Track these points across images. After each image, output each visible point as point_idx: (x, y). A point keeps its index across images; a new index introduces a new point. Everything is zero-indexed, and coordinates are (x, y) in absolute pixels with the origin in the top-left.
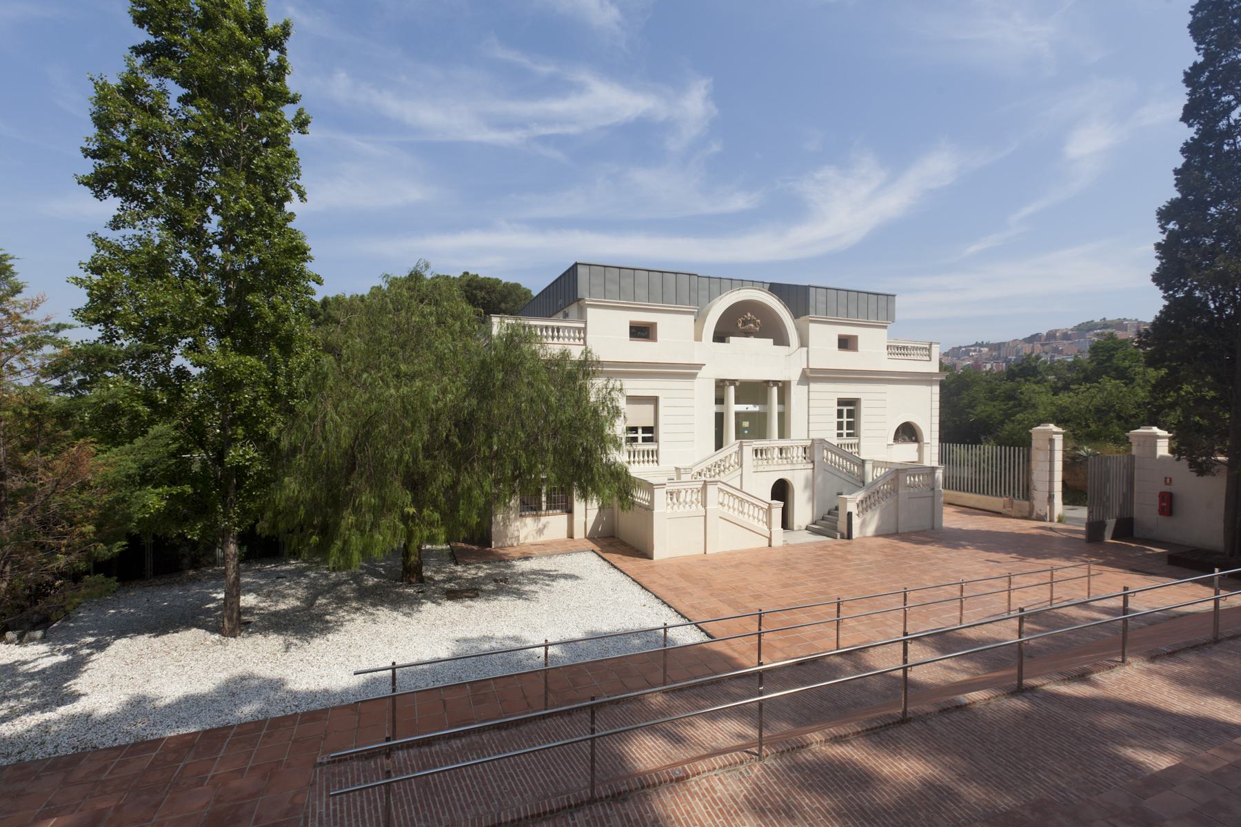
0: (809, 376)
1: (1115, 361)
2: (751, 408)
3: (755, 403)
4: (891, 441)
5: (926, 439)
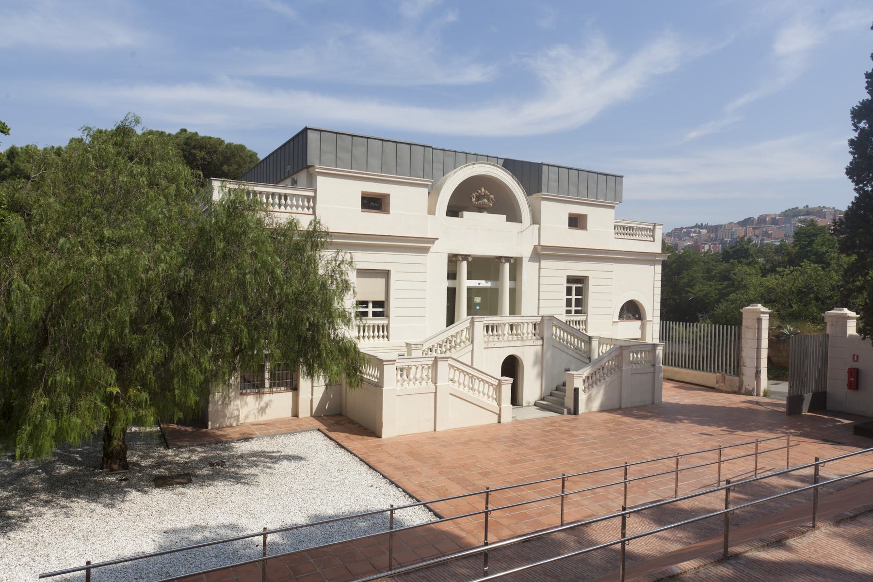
0: (540, 254)
1: (814, 246)
2: (483, 284)
3: (487, 279)
4: (616, 319)
5: (649, 317)
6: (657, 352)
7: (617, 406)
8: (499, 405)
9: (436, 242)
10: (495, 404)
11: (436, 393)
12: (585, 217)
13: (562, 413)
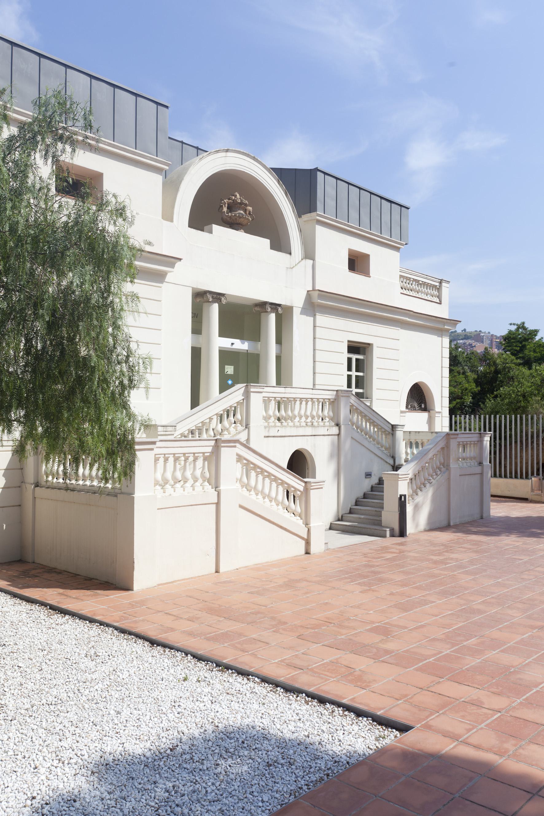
0: (320, 303)
1: (526, 352)
2: (240, 345)
3: (242, 338)
4: (404, 408)
5: (438, 408)
6: (485, 442)
7: (445, 523)
8: (307, 524)
9: (178, 264)
10: (300, 522)
11: (218, 504)
12: (366, 257)
13: (384, 536)
